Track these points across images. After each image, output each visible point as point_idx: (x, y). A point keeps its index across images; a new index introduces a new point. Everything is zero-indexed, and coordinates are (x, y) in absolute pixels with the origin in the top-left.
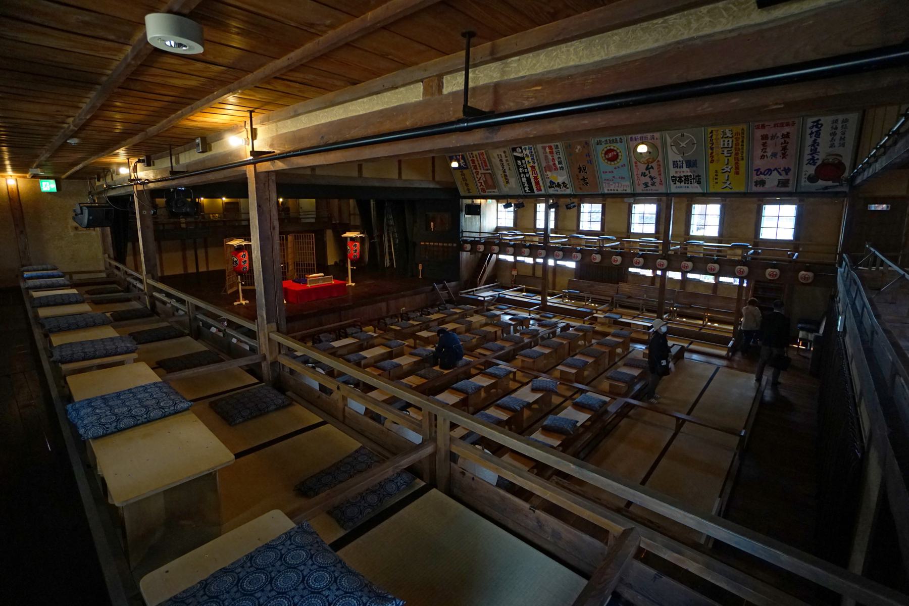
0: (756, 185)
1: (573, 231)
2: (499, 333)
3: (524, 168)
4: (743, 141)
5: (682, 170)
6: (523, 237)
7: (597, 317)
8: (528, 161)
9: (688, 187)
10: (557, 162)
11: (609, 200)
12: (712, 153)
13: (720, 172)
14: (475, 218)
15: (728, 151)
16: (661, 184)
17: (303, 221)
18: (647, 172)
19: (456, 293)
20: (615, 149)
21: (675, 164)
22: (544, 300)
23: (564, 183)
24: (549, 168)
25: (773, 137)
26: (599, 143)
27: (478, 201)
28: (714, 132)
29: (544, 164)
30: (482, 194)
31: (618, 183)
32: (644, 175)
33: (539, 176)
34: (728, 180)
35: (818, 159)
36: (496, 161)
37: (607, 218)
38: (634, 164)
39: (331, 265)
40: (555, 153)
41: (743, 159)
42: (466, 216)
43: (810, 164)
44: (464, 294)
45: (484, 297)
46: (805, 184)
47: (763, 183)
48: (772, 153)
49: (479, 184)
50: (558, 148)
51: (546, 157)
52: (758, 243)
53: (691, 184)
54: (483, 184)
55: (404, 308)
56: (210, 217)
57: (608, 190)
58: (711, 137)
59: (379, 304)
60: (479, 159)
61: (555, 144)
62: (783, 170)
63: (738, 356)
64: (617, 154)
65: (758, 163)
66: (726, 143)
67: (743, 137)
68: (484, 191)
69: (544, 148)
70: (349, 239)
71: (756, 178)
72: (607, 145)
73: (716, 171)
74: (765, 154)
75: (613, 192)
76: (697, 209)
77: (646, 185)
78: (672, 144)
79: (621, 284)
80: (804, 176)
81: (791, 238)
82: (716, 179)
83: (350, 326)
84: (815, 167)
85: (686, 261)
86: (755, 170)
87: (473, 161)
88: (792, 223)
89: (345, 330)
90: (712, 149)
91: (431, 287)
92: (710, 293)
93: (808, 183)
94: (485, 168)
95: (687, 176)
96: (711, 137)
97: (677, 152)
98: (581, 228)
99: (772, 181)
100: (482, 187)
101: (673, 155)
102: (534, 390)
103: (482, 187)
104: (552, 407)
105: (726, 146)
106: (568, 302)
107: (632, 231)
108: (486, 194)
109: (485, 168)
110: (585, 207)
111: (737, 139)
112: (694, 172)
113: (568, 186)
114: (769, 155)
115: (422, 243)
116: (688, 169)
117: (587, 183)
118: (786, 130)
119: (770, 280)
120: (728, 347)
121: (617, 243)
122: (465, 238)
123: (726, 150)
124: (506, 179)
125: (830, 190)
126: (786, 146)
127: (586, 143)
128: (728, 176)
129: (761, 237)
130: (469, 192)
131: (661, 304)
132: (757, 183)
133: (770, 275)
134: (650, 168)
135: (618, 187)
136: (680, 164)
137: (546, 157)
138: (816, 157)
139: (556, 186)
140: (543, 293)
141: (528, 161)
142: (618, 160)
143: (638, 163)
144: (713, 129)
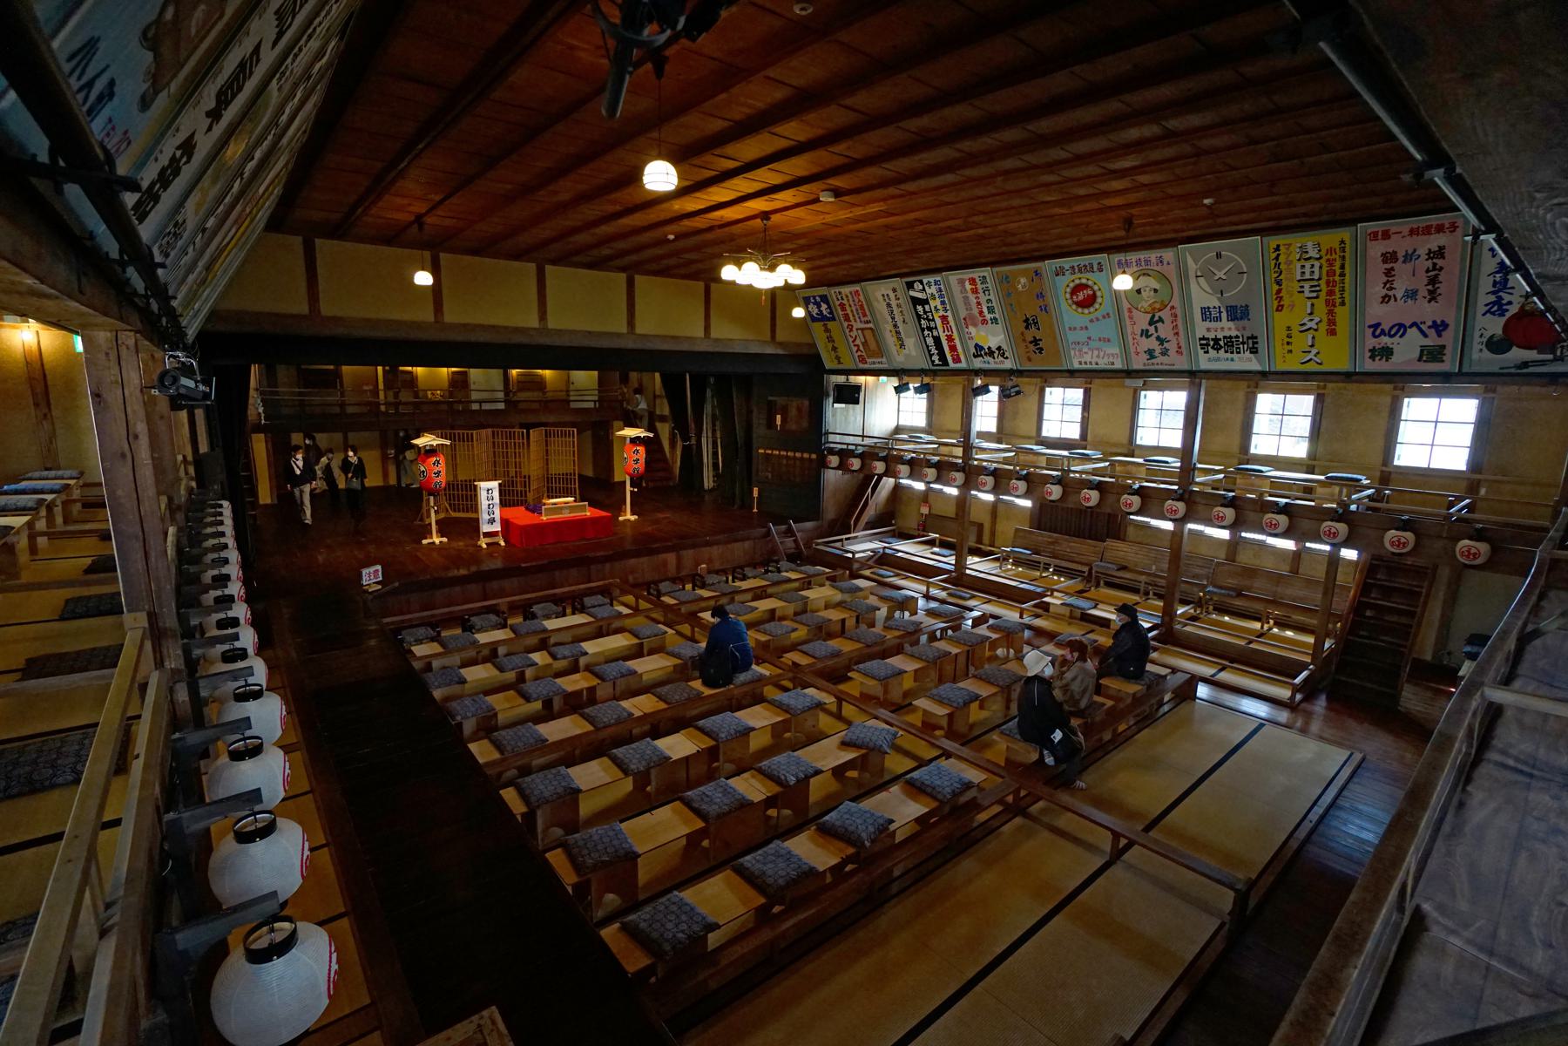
0: (1372, 357)
1: (1029, 438)
2: (850, 623)
3: (929, 320)
4: (1342, 267)
5: (1218, 325)
6: (936, 446)
7: (1048, 604)
8: (936, 307)
9: (1232, 360)
10: (985, 310)
11: (1097, 381)
12: (1279, 291)
13: (1296, 329)
14: (854, 409)
15: (1312, 286)
16: (1179, 352)
17: (573, 405)
18: (1152, 330)
19: (808, 544)
20: (1090, 283)
21: (1206, 314)
22: (960, 564)
23: (999, 348)
24: (969, 321)
25: (1408, 258)
26: (1059, 272)
27: (861, 379)
28: (1281, 248)
29: (963, 313)
30: (861, 366)
31: (1098, 349)
32: (1145, 334)
33: (955, 335)
34: (1312, 346)
35: (1510, 303)
36: (881, 307)
37: (1093, 414)
38: (1126, 314)
39: (1316, 433)
40: (981, 291)
41: (1343, 304)
42: (836, 405)
43: (1493, 314)
44: (820, 545)
45: (853, 553)
46: (1481, 358)
47: (1387, 353)
48: (1407, 291)
49: (855, 349)
50: (986, 282)
51: (966, 299)
52: (1388, 475)
53: (1239, 353)
54: (861, 348)
55: (704, 566)
56: (427, 396)
57: (1080, 363)
58: (1277, 258)
59: (664, 556)
60: (851, 303)
61: (982, 274)
62: (1429, 327)
63: (1320, 705)
64: (1094, 294)
65: (1377, 312)
66: (1307, 270)
67: (1343, 258)
68: (863, 360)
69: (962, 282)
70: (628, 440)
71: (1371, 342)
72: (1073, 277)
73: (1289, 328)
74: (1391, 293)
75: (1088, 367)
76: (1266, 402)
77: (1151, 353)
78: (1199, 274)
79: (1110, 543)
80: (1477, 339)
81: (1463, 467)
82: (1288, 343)
83: (592, 592)
84: (1504, 319)
85: (1222, 505)
86: (1370, 327)
87: (843, 309)
88: (1465, 435)
89: (582, 600)
90: (1279, 283)
91: (764, 530)
92: (1284, 570)
93: (1487, 354)
94: (863, 319)
95: (1231, 337)
96: (1277, 258)
97: (1208, 289)
98: (1044, 433)
99: (1406, 350)
100: (859, 353)
101: (1201, 296)
102: (845, 744)
103: (859, 353)
104: (887, 777)
105: (1307, 276)
106: (1011, 570)
107: (1138, 442)
108: (866, 366)
109: (863, 319)
110: (1054, 395)
111: (1331, 263)
112: (1244, 329)
113: (1007, 354)
114: (1399, 296)
115: (761, 451)
116: (1231, 324)
117: (1041, 349)
118: (1435, 242)
119: (1393, 553)
120: (1293, 685)
121: (1102, 465)
122: (832, 445)
123: (1307, 286)
124: (900, 339)
125: (1531, 370)
126: (1436, 276)
127: (1036, 273)
128: (1313, 338)
129: (1396, 463)
130: (839, 363)
131: (1172, 585)
132: (1374, 354)
133: (1392, 544)
134: (1157, 322)
135: (1098, 356)
136: (1214, 314)
137: (966, 299)
138: (1506, 298)
139: (986, 354)
140: (960, 550)
141: (936, 307)
142: (1097, 306)
143: (1134, 311)
144: (1281, 242)
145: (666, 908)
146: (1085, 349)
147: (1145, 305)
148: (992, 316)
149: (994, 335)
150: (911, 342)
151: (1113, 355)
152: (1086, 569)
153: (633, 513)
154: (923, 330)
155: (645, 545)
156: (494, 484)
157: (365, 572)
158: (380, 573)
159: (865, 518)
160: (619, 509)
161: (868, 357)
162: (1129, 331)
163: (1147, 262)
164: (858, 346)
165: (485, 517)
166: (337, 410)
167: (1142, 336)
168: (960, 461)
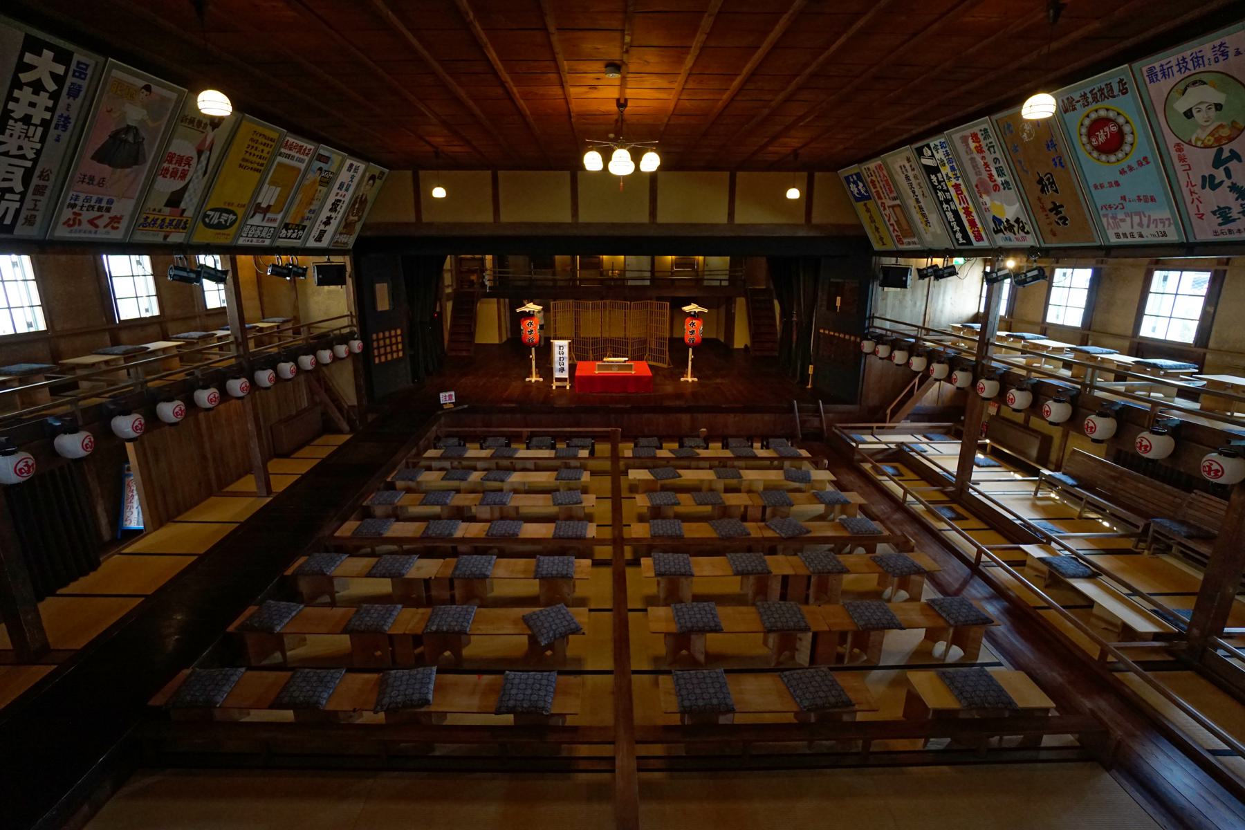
8: (947, 175)
10: (994, 172)
17: (706, 283)
18: (1220, 174)
19: (830, 426)
20: (1111, 115)
23: (1017, 221)
29: (974, 180)
31: (1138, 214)
32: (1210, 182)
33: (972, 208)
38: (1174, 154)
40: (985, 149)
54: (896, 228)
57: (1118, 236)
60: (879, 179)
69: (964, 140)
72: (1088, 109)
75: (1129, 240)
77: (1223, 214)
106: (1053, 500)
130: (884, 244)
134: (1229, 159)
135: (1141, 224)
142: (1127, 148)
143: (1186, 147)
145: (696, 699)
146: (1120, 216)
147: (1203, 135)
148: (1003, 179)
149: (1010, 204)
150: (934, 218)
151: (1162, 221)
152: (1141, 523)
153: (693, 375)
154: (941, 203)
155: (694, 404)
156: (565, 343)
157: (442, 395)
158: (454, 398)
159: (909, 408)
160: (684, 374)
161: (904, 237)
162: (1183, 180)
163: (1198, 59)
164: (892, 225)
165: (557, 366)
166: (551, 284)
167: (1203, 187)
168: (973, 359)
